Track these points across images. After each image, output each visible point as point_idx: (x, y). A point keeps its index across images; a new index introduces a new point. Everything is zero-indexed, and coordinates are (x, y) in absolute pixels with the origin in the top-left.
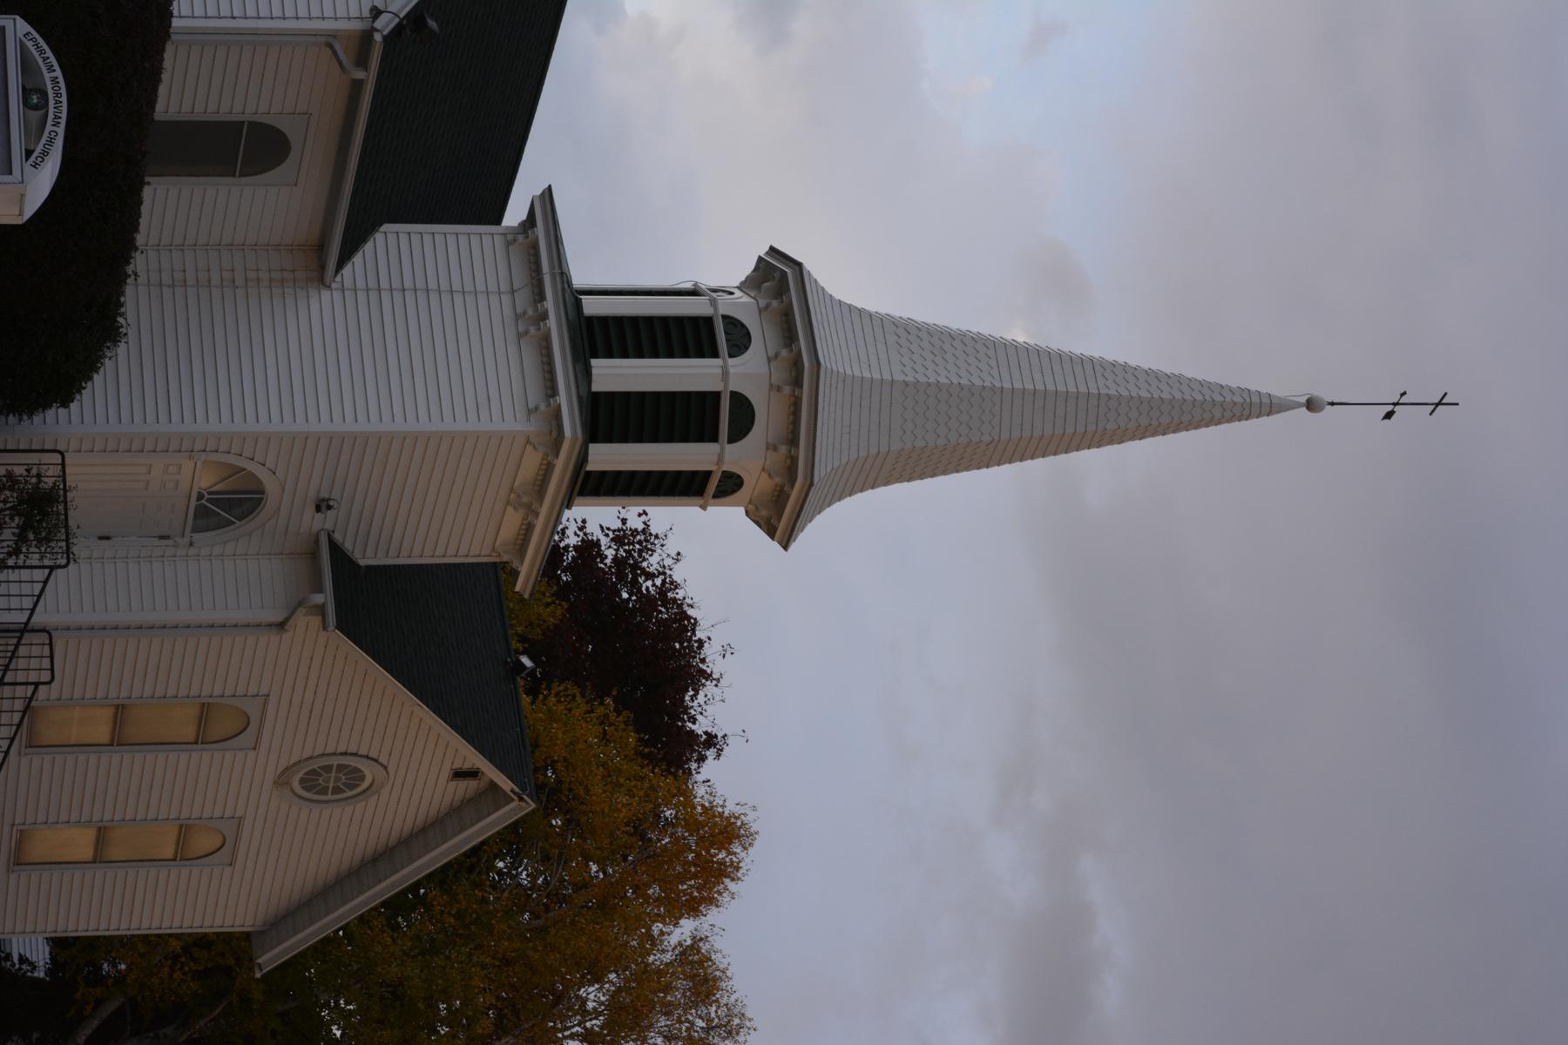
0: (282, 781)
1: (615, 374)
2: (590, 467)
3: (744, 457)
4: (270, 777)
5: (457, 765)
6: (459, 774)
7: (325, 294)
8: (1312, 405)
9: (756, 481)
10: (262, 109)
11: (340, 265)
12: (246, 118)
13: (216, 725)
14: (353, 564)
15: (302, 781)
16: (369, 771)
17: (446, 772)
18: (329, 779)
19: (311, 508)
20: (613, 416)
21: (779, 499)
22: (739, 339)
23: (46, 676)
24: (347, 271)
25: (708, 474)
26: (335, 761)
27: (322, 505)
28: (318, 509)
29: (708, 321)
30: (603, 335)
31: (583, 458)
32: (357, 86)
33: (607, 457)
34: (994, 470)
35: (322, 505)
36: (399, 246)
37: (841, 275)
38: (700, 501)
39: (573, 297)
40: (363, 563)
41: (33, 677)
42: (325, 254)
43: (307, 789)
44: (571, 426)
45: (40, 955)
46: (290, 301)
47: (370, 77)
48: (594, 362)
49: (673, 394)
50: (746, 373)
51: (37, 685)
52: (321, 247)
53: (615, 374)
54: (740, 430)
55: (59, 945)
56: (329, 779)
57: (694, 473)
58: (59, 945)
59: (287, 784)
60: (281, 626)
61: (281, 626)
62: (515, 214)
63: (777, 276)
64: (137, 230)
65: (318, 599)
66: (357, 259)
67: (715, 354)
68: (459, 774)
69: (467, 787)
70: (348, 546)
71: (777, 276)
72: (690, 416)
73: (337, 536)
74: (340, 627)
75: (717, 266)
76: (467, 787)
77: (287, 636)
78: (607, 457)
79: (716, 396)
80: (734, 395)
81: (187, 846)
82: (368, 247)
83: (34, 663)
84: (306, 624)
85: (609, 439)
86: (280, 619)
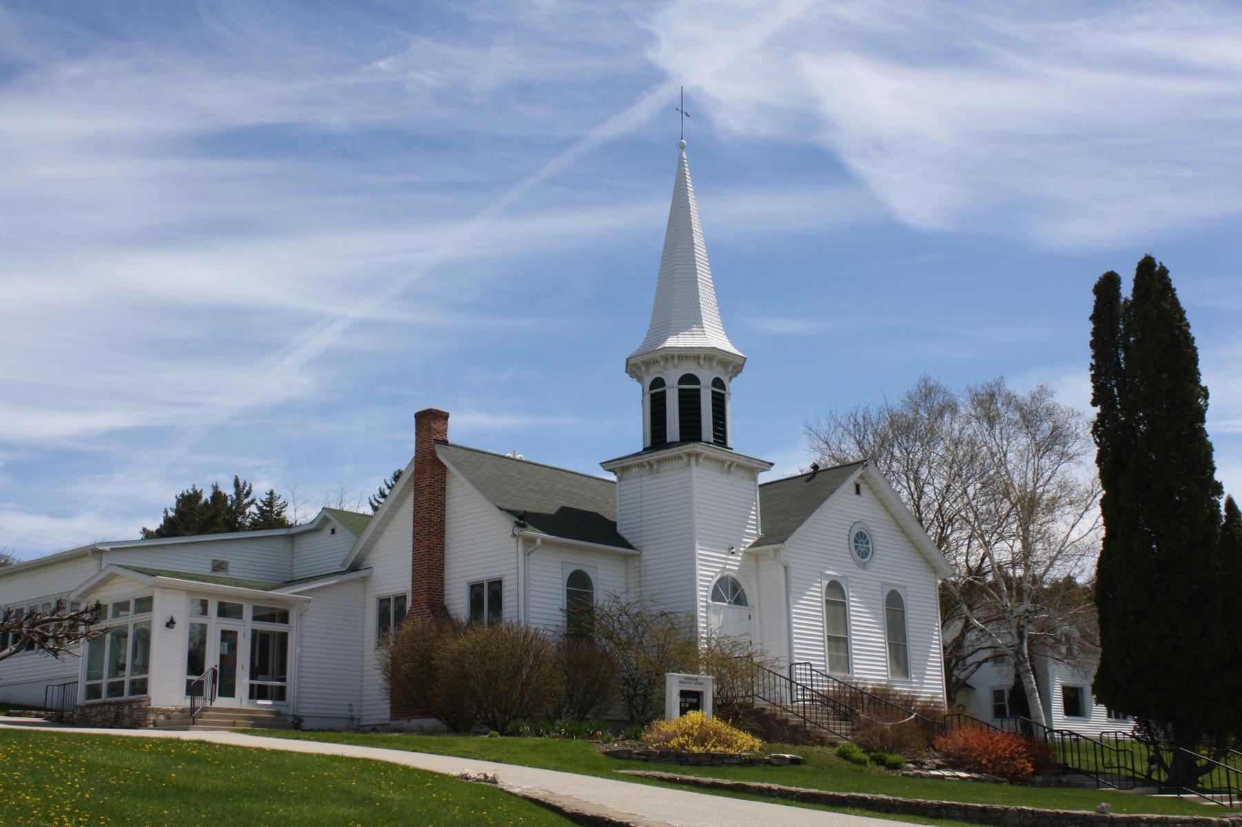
0: (864, 566)
3: (705, 377)
4: (862, 571)
6: (858, 492)
16: (855, 531)
17: (857, 497)
20: (691, 432)
22: (658, 382)
24: (635, 545)
25: (713, 392)
26: (853, 544)
29: (652, 395)
30: (658, 439)
32: (544, 542)
39: (646, 450)
45: (1098, 409)
48: (669, 440)
52: (626, 557)
55: (1094, 404)
57: (713, 398)
58: (1094, 404)
64: (465, 777)
66: (630, 541)
67: (664, 392)
68: (858, 492)
72: (689, 401)
79: (680, 390)
82: (626, 537)
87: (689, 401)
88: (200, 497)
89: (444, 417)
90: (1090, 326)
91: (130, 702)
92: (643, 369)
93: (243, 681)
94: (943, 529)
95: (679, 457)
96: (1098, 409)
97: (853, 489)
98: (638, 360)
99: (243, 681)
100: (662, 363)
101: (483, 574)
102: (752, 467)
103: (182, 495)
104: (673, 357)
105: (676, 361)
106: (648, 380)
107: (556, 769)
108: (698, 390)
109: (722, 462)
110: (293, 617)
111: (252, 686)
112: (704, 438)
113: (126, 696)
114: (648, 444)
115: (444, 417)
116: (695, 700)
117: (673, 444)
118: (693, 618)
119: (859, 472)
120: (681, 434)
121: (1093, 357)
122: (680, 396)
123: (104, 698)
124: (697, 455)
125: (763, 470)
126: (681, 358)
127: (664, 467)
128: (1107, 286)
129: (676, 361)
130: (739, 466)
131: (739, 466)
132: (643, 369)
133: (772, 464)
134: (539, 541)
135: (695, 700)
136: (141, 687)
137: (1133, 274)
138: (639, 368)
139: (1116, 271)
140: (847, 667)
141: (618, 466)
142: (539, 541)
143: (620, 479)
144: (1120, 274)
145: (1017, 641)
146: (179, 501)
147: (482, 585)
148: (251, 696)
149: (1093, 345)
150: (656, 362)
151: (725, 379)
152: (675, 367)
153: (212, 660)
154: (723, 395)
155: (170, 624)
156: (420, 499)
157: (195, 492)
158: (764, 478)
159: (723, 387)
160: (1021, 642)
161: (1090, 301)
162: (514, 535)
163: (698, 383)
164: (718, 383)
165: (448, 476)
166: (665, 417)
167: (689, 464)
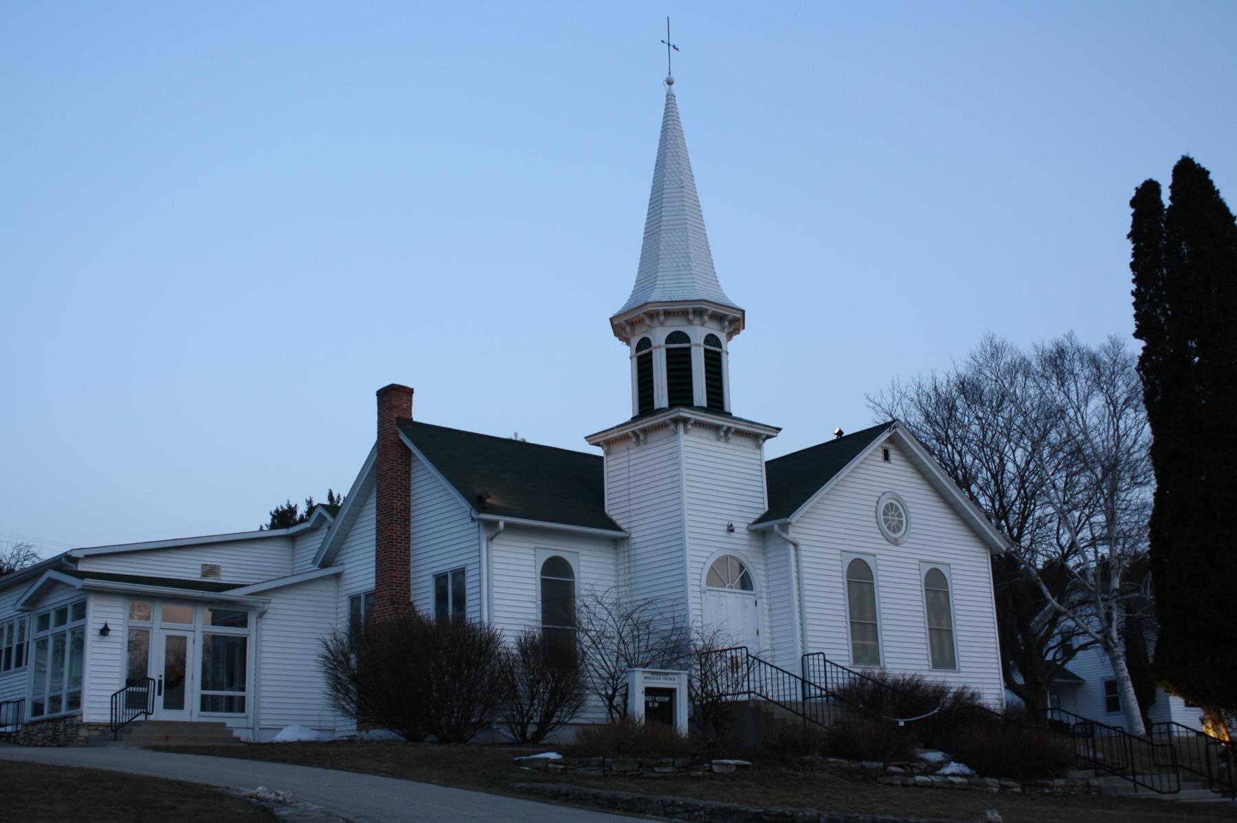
0: (895, 542)
1: (661, 398)
2: (705, 404)
3: (697, 334)
5: (881, 459)
7: (633, 535)
8: (670, 83)
9: (712, 328)
10: (533, 569)
11: (618, 529)
12: (539, 577)
13: (860, 578)
14: (767, 514)
15: (894, 532)
17: (886, 465)
18: (892, 519)
19: (732, 534)
21: (719, 318)
22: (645, 343)
23: (821, 657)
24: (623, 527)
25: (706, 350)
27: (731, 529)
28: (732, 531)
31: (701, 409)
32: (507, 525)
33: (700, 395)
34: (1124, 282)
35: (731, 529)
36: (613, 506)
37: (619, 298)
38: (724, 355)
40: (767, 509)
41: (822, 663)
42: (615, 538)
43: (899, 530)
44: (685, 413)
46: (638, 552)
47: (502, 520)
48: (656, 407)
49: (690, 369)
50: (659, 336)
51: (825, 661)
53: (661, 398)
54: (684, 338)
55: (1137, 335)
56: (892, 519)
58: (1137, 335)
59: (896, 539)
60: (795, 545)
61: (795, 545)
62: (598, 451)
63: (623, 326)
65: (776, 528)
66: (619, 522)
67: (650, 354)
69: (893, 455)
70: (757, 516)
71: (623, 326)
72: (679, 361)
73: (751, 521)
74: (788, 516)
75: (622, 356)
76: (893, 455)
77: (801, 542)
78: (700, 395)
79: (668, 350)
80: (667, 342)
81: (936, 586)
82: (614, 518)
83: (816, 662)
84: (792, 535)
85: (691, 398)
86: (792, 547)
87: (679, 361)
88: (295, 512)
89: (408, 392)
90: (1129, 246)
91: (66, 717)
92: (628, 329)
93: (193, 689)
94: (1025, 504)
95: (664, 425)
96: (1142, 343)
97: (881, 454)
98: (622, 320)
99: (193, 689)
100: (647, 321)
101: (447, 564)
102: (757, 434)
103: (277, 511)
104: (658, 314)
105: (662, 318)
106: (635, 341)
107: (448, 782)
108: (689, 349)
109: (716, 428)
110: (252, 620)
111: (204, 698)
112: (696, 403)
113: (64, 711)
114: (637, 413)
115: (408, 392)
116: (667, 699)
117: (661, 410)
118: (682, 601)
119: (886, 435)
120: (670, 399)
121: (1134, 281)
122: (668, 357)
123: (46, 715)
124: (685, 421)
125: (769, 437)
126: (667, 314)
127: (652, 437)
128: (1146, 194)
129: (662, 318)
130: (739, 433)
131: (739, 433)
132: (628, 329)
133: (779, 429)
134: (502, 525)
135: (667, 699)
136: (75, 701)
137: (1170, 181)
138: (624, 329)
139: (1155, 179)
140: (875, 659)
141: (608, 439)
142: (502, 525)
143: (607, 453)
144: (1147, 178)
145: (1105, 623)
146: (274, 517)
147: (446, 577)
148: (204, 708)
149: (1132, 265)
150: (641, 321)
151: (722, 336)
152: (662, 324)
153: (156, 669)
154: (719, 354)
155: (105, 631)
156: (383, 485)
157: (290, 507)
158: (774, 449)
159: (719, 345)
160: (1110, 625)
161: (1125, 218)
162: (473, 520)
163: (689, 341)
164: (711, 340)
165: (413, 459)
166: (652, 381)
167: (676, 432)
